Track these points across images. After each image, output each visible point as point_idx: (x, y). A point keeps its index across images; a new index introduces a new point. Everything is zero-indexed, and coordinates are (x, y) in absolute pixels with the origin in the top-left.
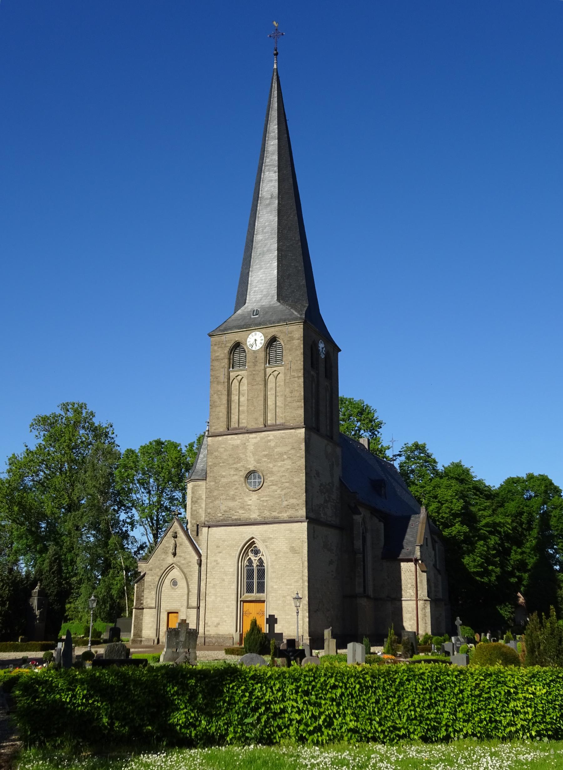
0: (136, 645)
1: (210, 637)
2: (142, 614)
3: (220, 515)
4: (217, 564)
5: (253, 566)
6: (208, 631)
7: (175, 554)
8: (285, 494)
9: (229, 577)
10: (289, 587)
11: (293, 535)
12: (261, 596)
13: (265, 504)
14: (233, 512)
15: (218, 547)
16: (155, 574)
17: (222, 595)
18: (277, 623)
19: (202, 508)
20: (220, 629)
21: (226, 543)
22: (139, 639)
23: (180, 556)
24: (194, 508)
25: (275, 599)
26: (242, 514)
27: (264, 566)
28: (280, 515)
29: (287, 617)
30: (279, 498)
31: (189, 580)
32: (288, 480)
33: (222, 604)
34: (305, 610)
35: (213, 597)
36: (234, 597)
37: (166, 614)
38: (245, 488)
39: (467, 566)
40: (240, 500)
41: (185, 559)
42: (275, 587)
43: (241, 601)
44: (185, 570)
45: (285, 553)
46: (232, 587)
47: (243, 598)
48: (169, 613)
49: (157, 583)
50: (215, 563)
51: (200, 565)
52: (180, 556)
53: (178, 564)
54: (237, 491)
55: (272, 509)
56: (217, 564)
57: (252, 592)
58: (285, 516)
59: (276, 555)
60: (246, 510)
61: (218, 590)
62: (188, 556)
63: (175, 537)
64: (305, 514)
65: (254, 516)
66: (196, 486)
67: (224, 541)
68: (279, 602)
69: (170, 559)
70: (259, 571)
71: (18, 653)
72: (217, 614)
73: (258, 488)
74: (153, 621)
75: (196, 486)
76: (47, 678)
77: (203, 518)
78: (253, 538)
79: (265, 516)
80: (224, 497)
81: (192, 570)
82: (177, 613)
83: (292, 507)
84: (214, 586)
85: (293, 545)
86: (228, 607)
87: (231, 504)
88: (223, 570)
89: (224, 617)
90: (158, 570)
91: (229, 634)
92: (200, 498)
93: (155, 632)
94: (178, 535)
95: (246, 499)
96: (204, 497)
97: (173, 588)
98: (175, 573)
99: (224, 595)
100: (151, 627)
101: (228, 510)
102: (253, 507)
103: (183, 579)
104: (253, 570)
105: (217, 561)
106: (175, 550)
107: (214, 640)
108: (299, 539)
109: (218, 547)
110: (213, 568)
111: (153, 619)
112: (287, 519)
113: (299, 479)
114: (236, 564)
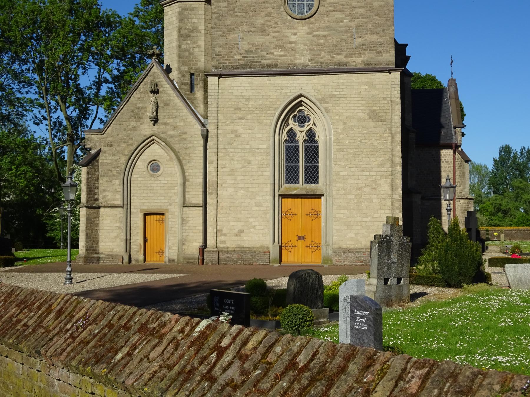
0: (91, 266)
1: (228, 252)
2: (98, 216)
3: (238, 57)
4: (237, 136)
5: (297, 142)
6: (224, 242)
7: (155, 120)
8: (358, 27)
10: (367, 173)
11: (375, 92)
12: (311, 187)
13: (322, 41)
14: (264, 53)
15: (238, 109)
16: (118, 152)
17: (247, 185)
18: (466, 217)
19: (199, 46)
20: (245, 238)
21: (251, 103)
22: (96, 256)
23: (166, 124)
24: (183, 46)
26: (279, 57)
27: (316, 142)
28: (350, 60)
29: (364, 219)
30: (347, 32)
31: (184, 162)
32: (363, 4)
34: (397, 208)
35: (231, 190)
36: (269, 188)
37: (141, 216)
38: (284, 14)
40: (276, 34)
41: (175, 128)
42: (342, 173)
43: (279, 195)
44: (176, 147)
45: (360, 120)
46: (265, 174)
47: (283, 191)
48: (146, 215)
49: (123, 167)
50: (233, 136)
51: (206, 138)
52: (166, 124)
53: (162, 136)
54: (269, 18)
55: (334, 50)
56: (237, 136)
57: (297, 181)
58: (358, 61)
59: (344, 124)
60: (287, 50)
61: (239, 178)
62: (182, 124)
63: (155, 92)
64: (393, 59)
65: (303, 60)
66: (187, 10)
67: (248, 100)
68: (350, 197)
69: (147, 128)
70: (306, 148)
71: (163, 275)
72: (239, 216)
73: (307, 15)
74: (120, 228)
75: (187, 10)
77: (201, 62)
78: (301, 96)
79: (322, 60)
80: (246, 28)
81: (189, 145)
82: (163, 214)
83: (372, 47)
84: (232, 172)
85: (374, 108)
86: (259, 205)
87: (259, 40)
88: (248, 147)
89: (251, 220)
90: (124, 145)
91: (261, 247)
92: (194, 29)
93: (123, 244)
94: (161, 90)
95: (287, 32)
96: (202, 28)
97: (152, 176)
98: (155, 151)
99: (250, 185)
100: (116, 237)
101: (253, 49)
102: (300, 46)
103: (171, 159)
104: (297, 148)
105: (236, 131)
106: (157, 113)
107: (235, 256)
108: (384, 99)
109: (238, 109)
110: (230, 143)
111: (118, 225)
112: (362, 66)
113: (383, 3)
114: (272, 137)
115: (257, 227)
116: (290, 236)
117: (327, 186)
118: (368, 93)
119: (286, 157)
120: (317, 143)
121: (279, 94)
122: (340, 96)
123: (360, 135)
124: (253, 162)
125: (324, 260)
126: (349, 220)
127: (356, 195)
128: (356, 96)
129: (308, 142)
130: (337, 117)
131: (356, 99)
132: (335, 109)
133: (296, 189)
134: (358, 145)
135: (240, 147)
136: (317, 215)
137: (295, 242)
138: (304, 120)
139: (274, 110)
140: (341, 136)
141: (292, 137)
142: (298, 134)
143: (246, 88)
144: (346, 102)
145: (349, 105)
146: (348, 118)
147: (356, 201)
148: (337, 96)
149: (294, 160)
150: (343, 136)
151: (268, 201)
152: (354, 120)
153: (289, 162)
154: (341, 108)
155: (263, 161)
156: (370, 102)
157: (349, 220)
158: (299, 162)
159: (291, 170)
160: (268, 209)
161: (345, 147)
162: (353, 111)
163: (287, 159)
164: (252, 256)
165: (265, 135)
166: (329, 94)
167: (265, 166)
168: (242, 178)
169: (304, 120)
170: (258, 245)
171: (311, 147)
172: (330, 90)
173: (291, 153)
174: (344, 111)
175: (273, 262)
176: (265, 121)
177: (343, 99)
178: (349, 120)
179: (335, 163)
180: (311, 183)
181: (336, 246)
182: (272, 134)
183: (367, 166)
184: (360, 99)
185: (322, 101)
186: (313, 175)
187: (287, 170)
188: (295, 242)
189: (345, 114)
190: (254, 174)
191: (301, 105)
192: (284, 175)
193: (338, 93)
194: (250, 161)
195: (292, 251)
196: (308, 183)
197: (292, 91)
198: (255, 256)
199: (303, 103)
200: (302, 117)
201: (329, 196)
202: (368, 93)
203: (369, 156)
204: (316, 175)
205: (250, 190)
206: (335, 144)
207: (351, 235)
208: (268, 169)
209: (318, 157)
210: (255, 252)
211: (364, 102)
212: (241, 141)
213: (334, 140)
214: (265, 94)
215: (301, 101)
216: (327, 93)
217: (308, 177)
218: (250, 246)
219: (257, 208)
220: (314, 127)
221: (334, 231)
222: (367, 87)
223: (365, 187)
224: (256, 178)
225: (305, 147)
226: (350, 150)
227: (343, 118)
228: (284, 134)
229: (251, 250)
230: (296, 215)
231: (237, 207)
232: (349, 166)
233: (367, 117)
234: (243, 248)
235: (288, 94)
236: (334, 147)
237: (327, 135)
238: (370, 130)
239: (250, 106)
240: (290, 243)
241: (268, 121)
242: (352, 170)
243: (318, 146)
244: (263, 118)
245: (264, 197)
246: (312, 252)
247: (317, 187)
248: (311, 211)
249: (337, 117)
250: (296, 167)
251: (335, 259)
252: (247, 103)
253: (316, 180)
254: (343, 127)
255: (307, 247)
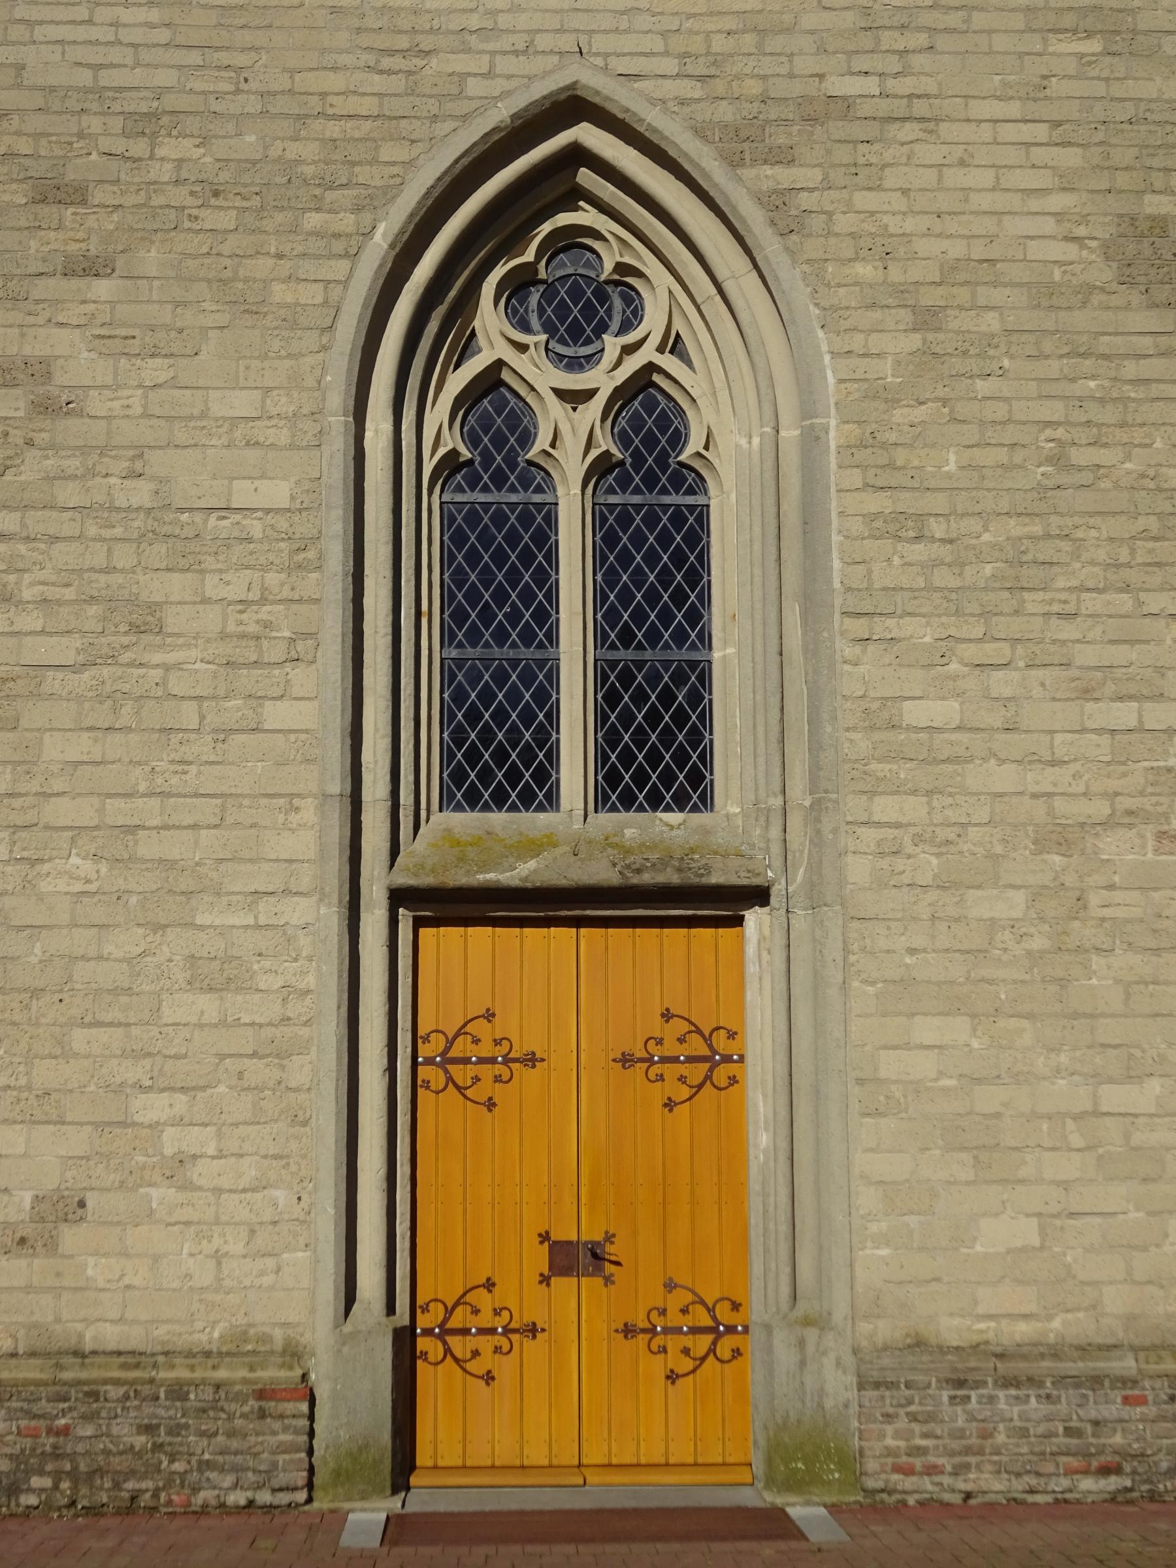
4: (45, 408)
5: (536, 476)
9: (237, 586)
10: (1125, 715)
12: (657, 836)
17: (118, 811)
20: (96, 1270)
21: (169, 149)
25: (929, 864)
27: (688, 479)
29: (1114, 1097)
33: (126, 942)
36: (306, 838)
39: (58, 1328)
42: (915, 713)
43: (398, 897)
46: (277, 714)
57: (534, 786)
59: (927, 320)
67: (147, 124)
68: (985, 905)
70: (611, 535)
72: (45, 1074)
76: (79, 1327)
78: (571, 107)
86: (221, 976)
88: (141, 494)
89: (152, 1108)
91: (238, 1347)
99: (150, 811)
104: (540, 528)
109: (57, 193)
114: (338, 422)
115: (204, 1173)
116: (483, 1241)
117: (795, 821)
118: (1100, 89)
119: (447, 597)
120: (698, 485)
121: (397, 83)
122: (884, 107)
123: (1054, 411)
124: (174, 620)
125: (776, 1451)
126: (989, 1099)
127: (1037, 894)
128: (1014, 109)
129: (624, 483)
130: (865, 271)
131: (1009, 132)
132: (849, 208)
133: (533, 847)
134: (1041, 490)
135: (69, 494)
136: (711, 1060)
137: (523, 1291)
138: (589, 311)
139: (358, 209)
140: (899, 415)
141: (499, 441)
142: (551, 415)
143: (136, 36)
144: (930, 153)
145: (955, 177)
146: (949, 273)
147: (1038, 943)
148: (865, 109)
149: (514, 617)
150: (920, 413)
151: (304, 941)
152: (998, 296)
153: (474, 637)
154: (898, 202)
155: (265, 612)
156: (1124, 156)
157: (989, 1099)
158: (552, 638)
159: (487, 697)
160: (296, 1009)
161: (939, 502)
162: (988, 225)
163: (459, 616)
164: (149, 1429)
165: (282, 404)
166: (797, 88)
167: (276, 653)
168: (81, 747)
169: (589, 311)
170: (209, 1333)
171: (651, 520)
172: (805, 65)
173: (490, 562)
174: (924, 222)
175: (340, 1476)
176: (280, 293)
177: (910, 131)
178: (963, 295)
179: (859, 627)
180: (655, 801)
181: (885, 1330)
182: (338, 398)
183: (1122, 654)
184: (1041, 132)
185: (743, 144)
186: (667, 737)
187: (459, 697)
188: (523, 1291)
189: (924, 247)
190: (189, 715)
191: (574, 196)
192: (434, 736)
193: (871, 85)
194: (153, 608)
195: (505, 1368)
196: (628, 801)
197: (505, 65)
198: (176, 1430)
199: (586, 177)
200: (576, 293)
201: (815, 905)
202: (1100, 89)
203: (1133, 576)
204: (696, 737)
205: (148, 847)
206: (855, 478)
207: (1006, 1231)
208: (301, 678)
209: (705, 598)
210: (178, 1392)
211: (1071, 158)
212: (84, 450)
213: (846, 448)
214: (284, 83)
215: (578, 155)
216: (780, 88)
217: (627, 758)
218: (135, 1338)
219: (207, 1006)
220: (667, 362)
221: (867, 1199)
222: (1094, 46)
223: (1107, 824)
224: (202, 747)
225: (600, 519)
226: (974, 525)
227: (914, 274)
228: (438, 413)
229: (145, 1381)
230: (531, 1060)
231: (36, 993)
232: (970, 652)
233: (1103, 274)
234: (78, 1353)
235: (474, 87)
236: (847, 505)
237: (787, 415)
238: (1130, 369)
239: (165, 172)
240: (483, 1299)
241: (312, 294)
242: (1001, 683)
243: (702, 515)
244: (262, 267)
245: (265, 908)
246: (672, 1377)
247: (706, 831)
248: (656, 1027)
249: (865, 271)
250: (527, 678)
251: (883, 1443)
252: (139, 148)
253: (696, 778)
254: (915, 341)
255: (628, 1331)
